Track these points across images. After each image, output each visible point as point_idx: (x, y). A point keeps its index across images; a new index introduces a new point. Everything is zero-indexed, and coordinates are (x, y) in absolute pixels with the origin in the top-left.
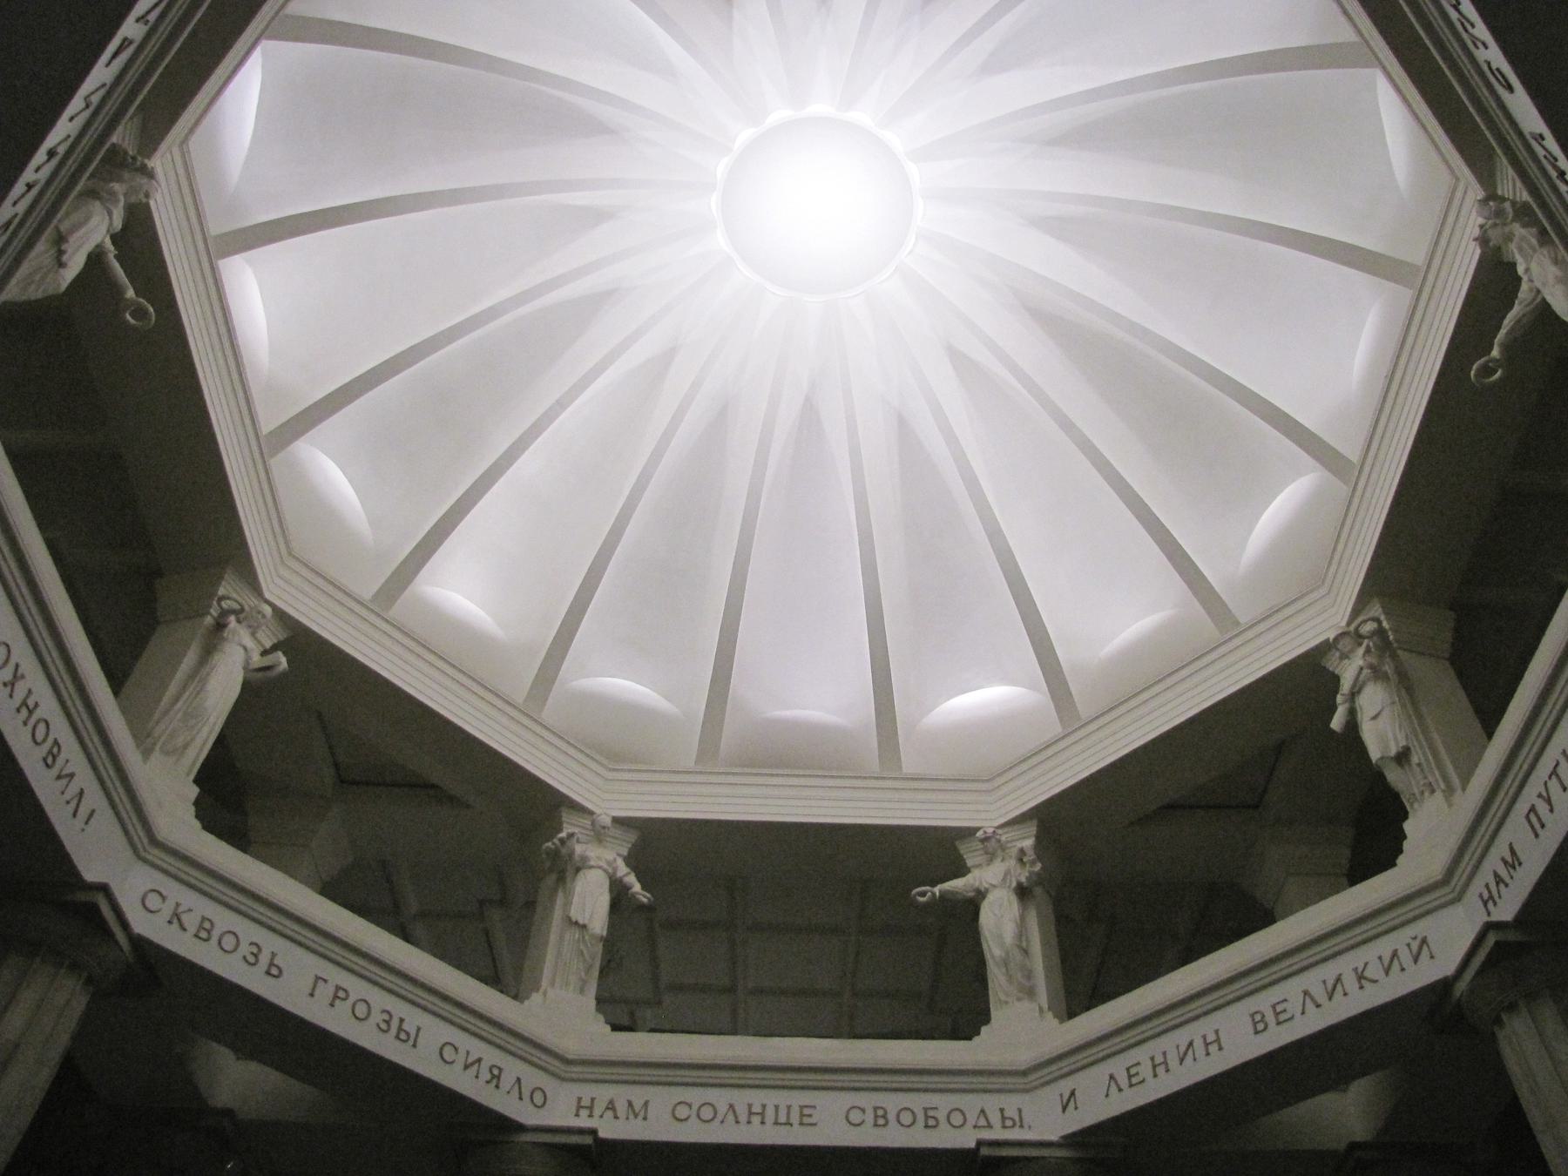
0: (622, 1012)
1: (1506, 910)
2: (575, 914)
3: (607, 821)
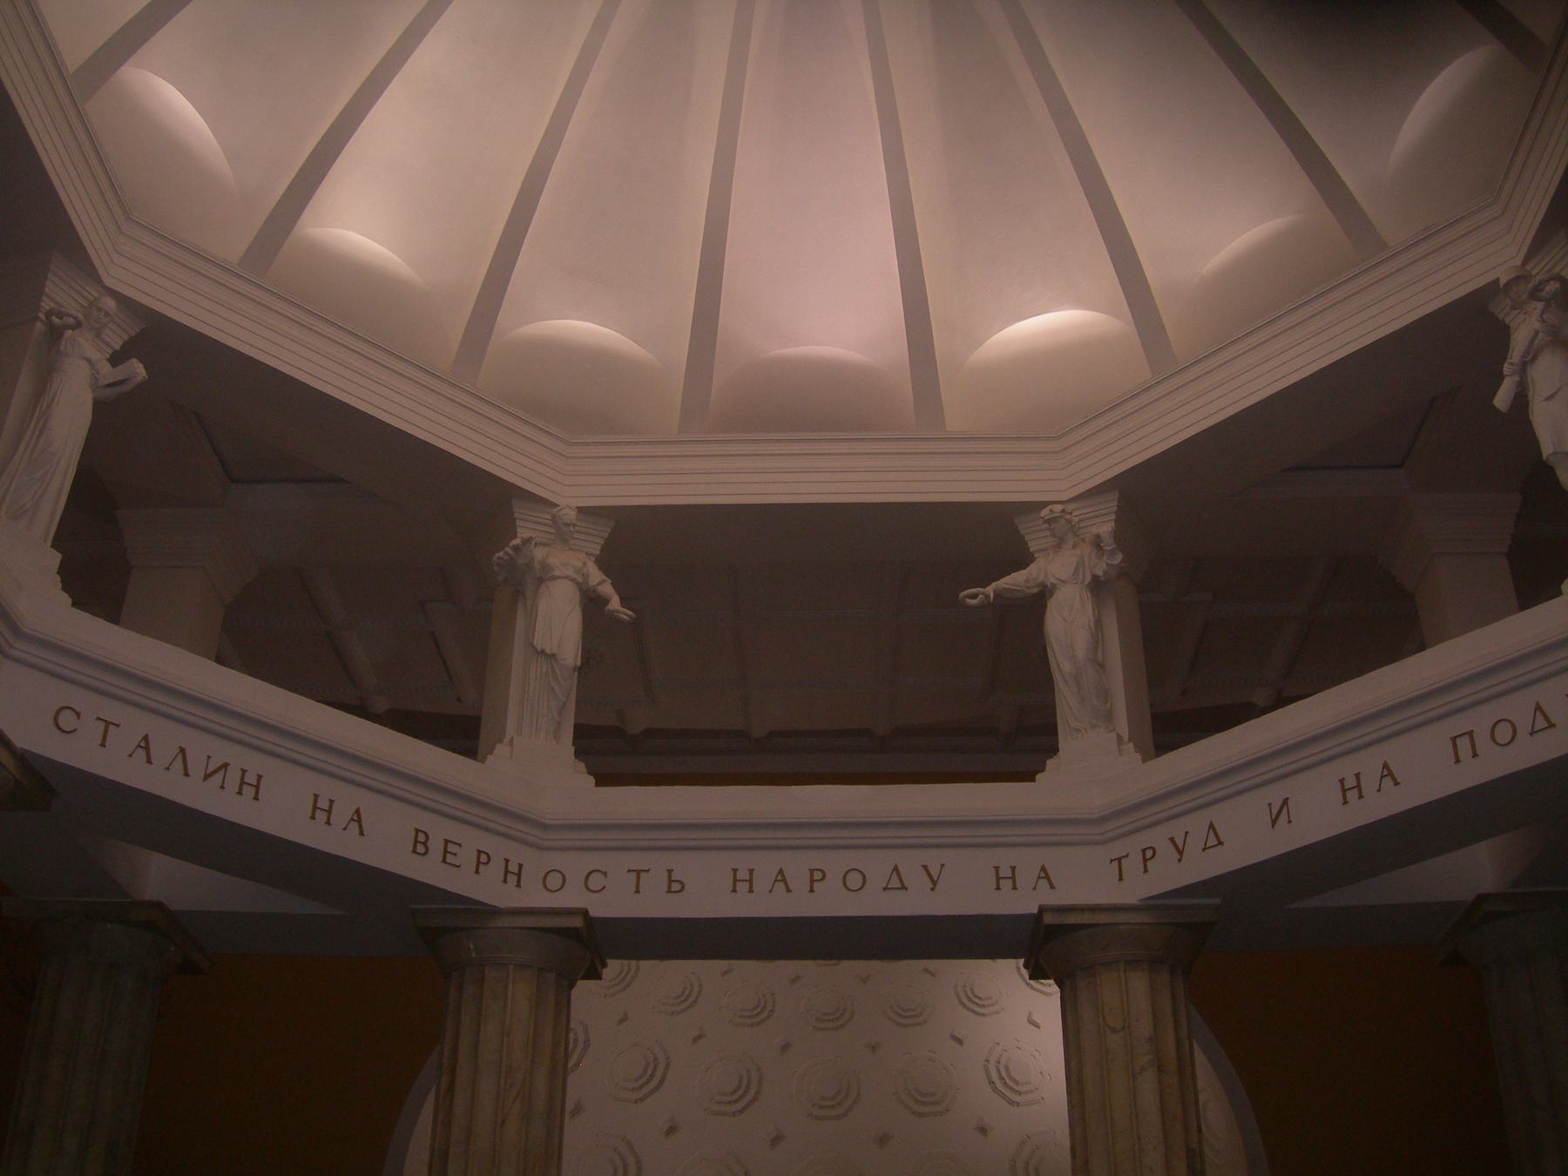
2: (540, 641)
3: (571, 515)
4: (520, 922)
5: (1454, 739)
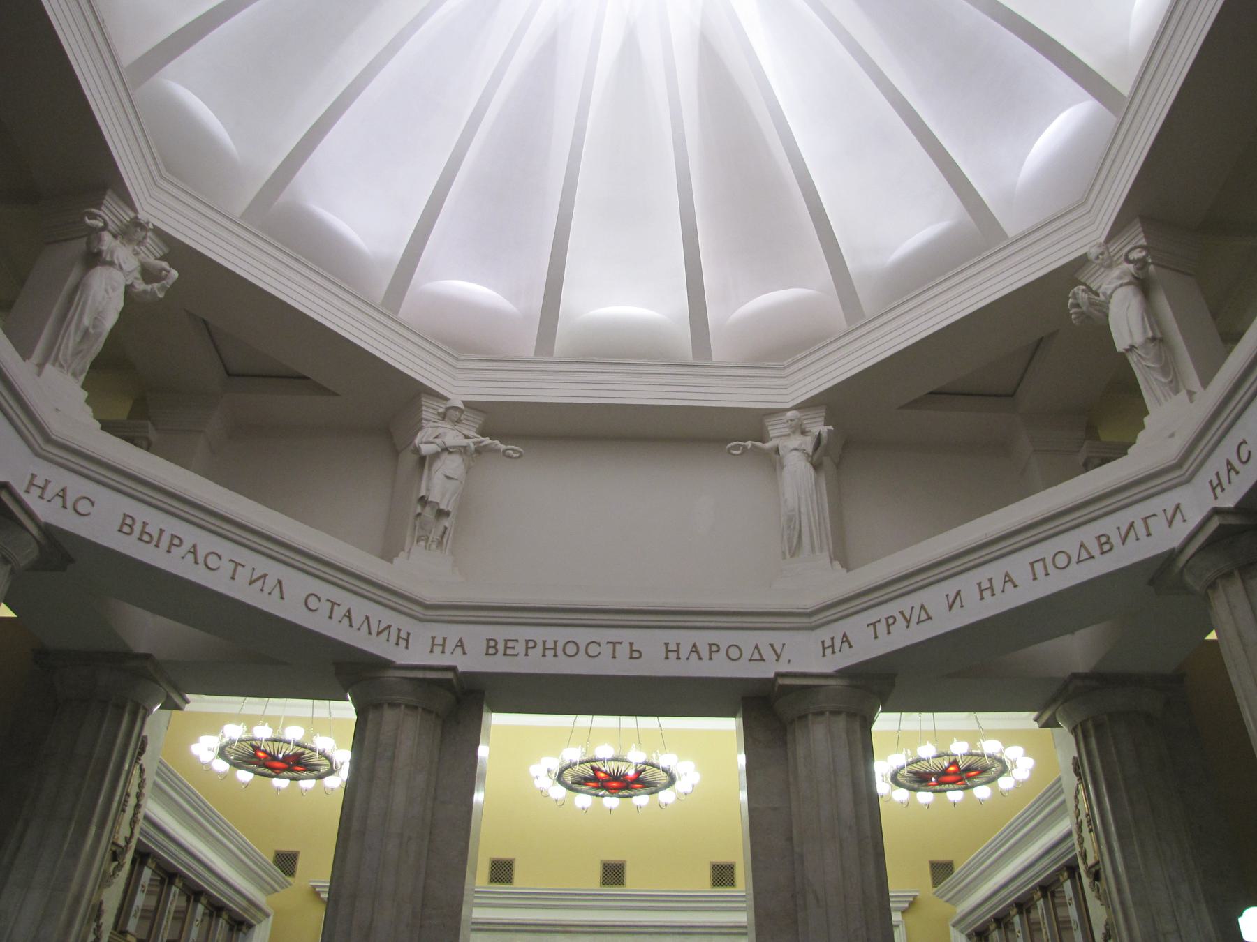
1: (1229, 500)
5: (1032, 564)
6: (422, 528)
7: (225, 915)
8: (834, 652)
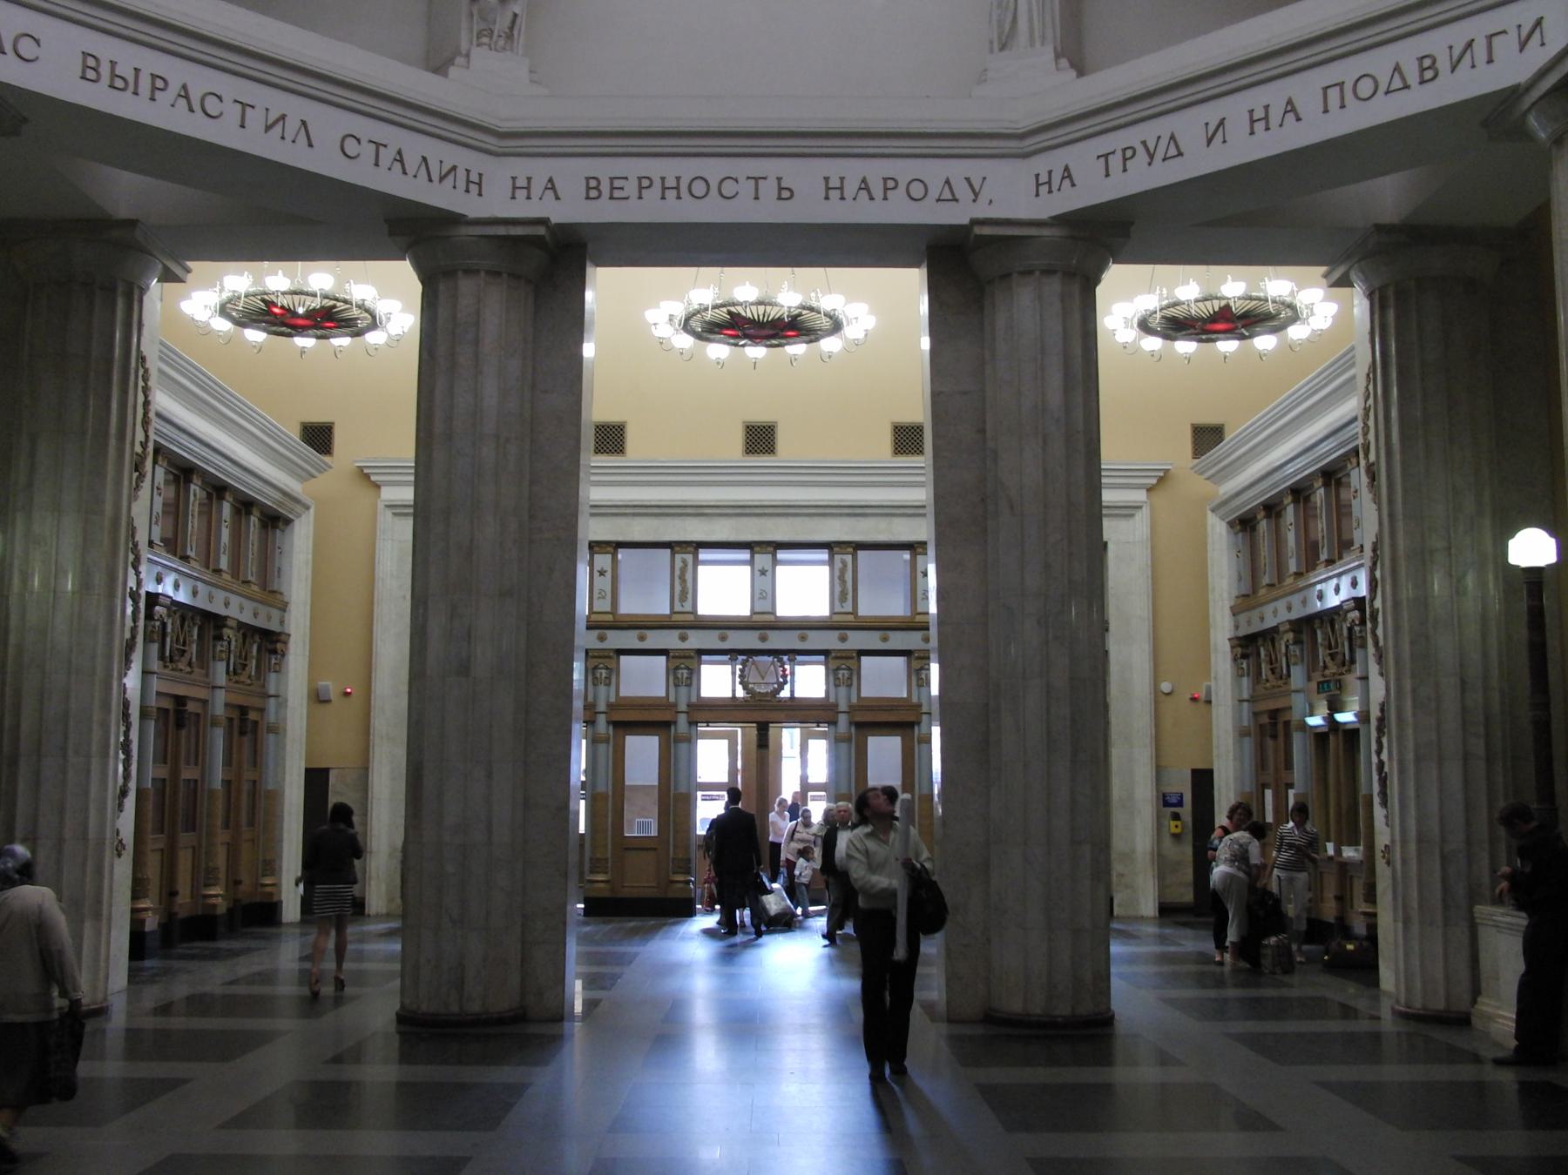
0: (355, 882)
4: (478, 231)
5: (1325, 89)
6: (484, 19)
7: (256, 512)
8: (1050, 192)
